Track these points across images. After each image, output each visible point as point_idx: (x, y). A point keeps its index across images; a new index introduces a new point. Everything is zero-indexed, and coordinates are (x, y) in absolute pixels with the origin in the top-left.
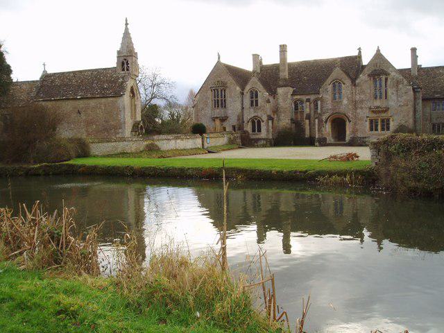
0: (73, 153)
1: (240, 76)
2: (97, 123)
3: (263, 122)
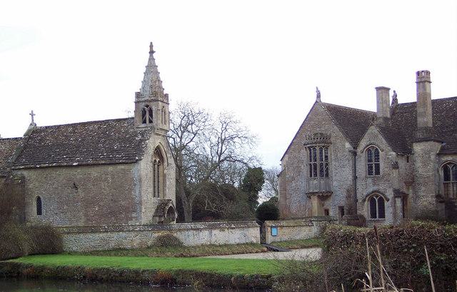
0: (26, 247)
1: (351, 121)
2: (101, 204)
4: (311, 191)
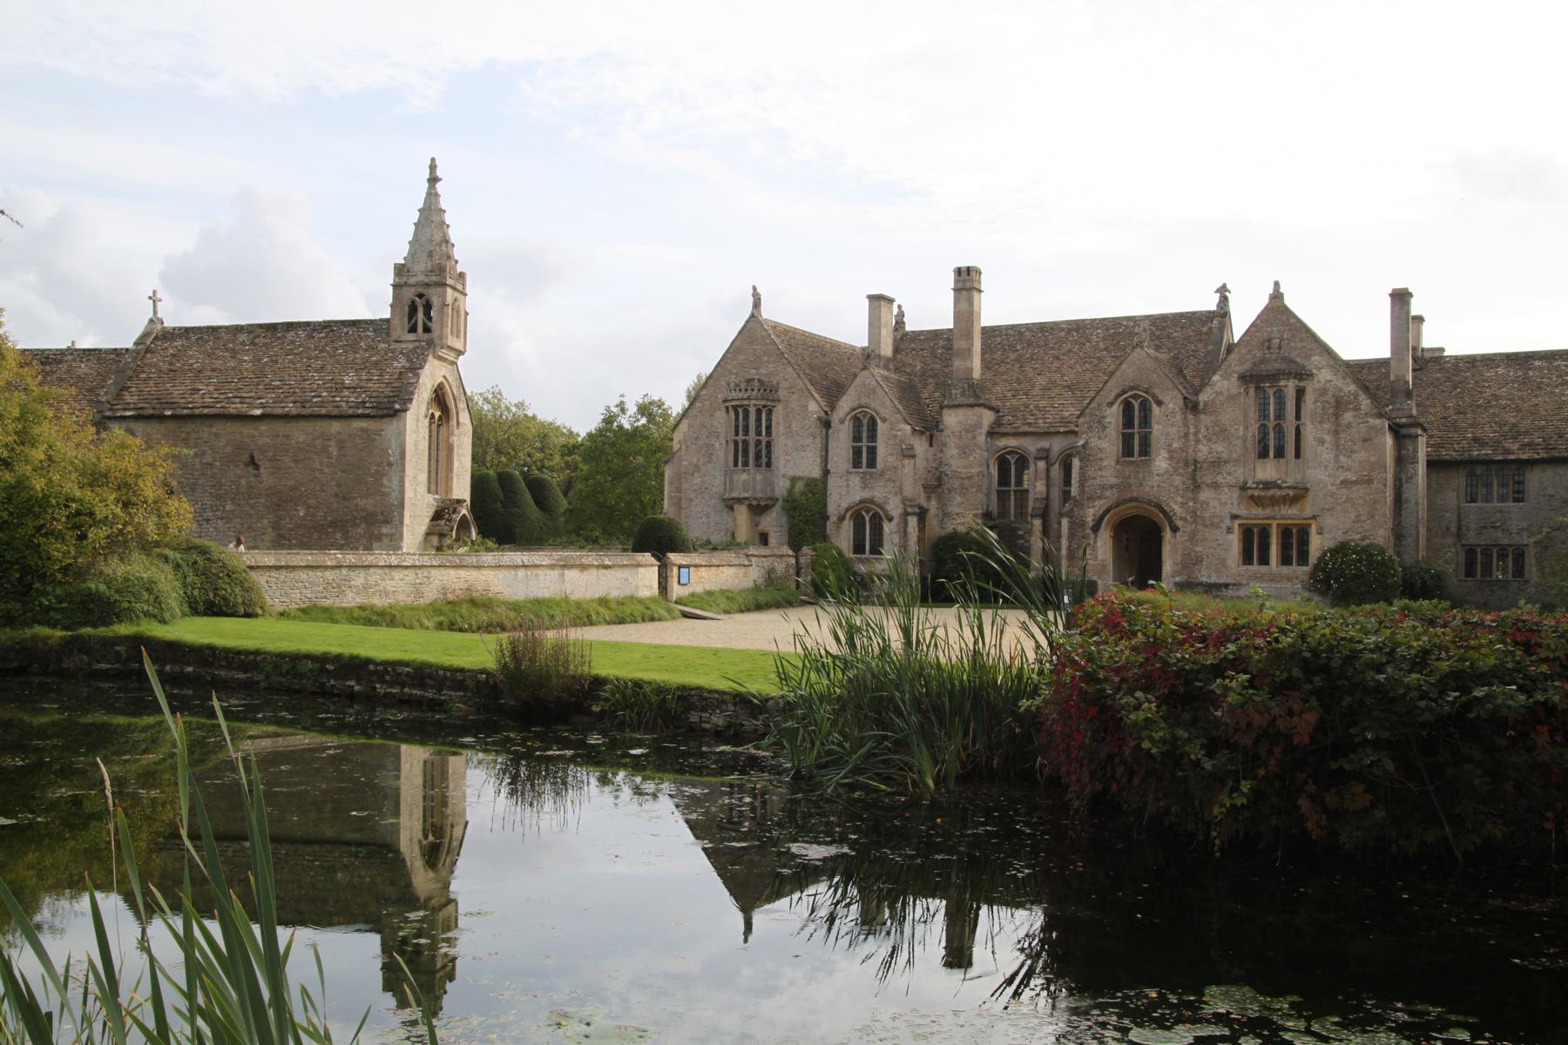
2: (312, 502)
3: (890, 519)
4: (735, 495)
